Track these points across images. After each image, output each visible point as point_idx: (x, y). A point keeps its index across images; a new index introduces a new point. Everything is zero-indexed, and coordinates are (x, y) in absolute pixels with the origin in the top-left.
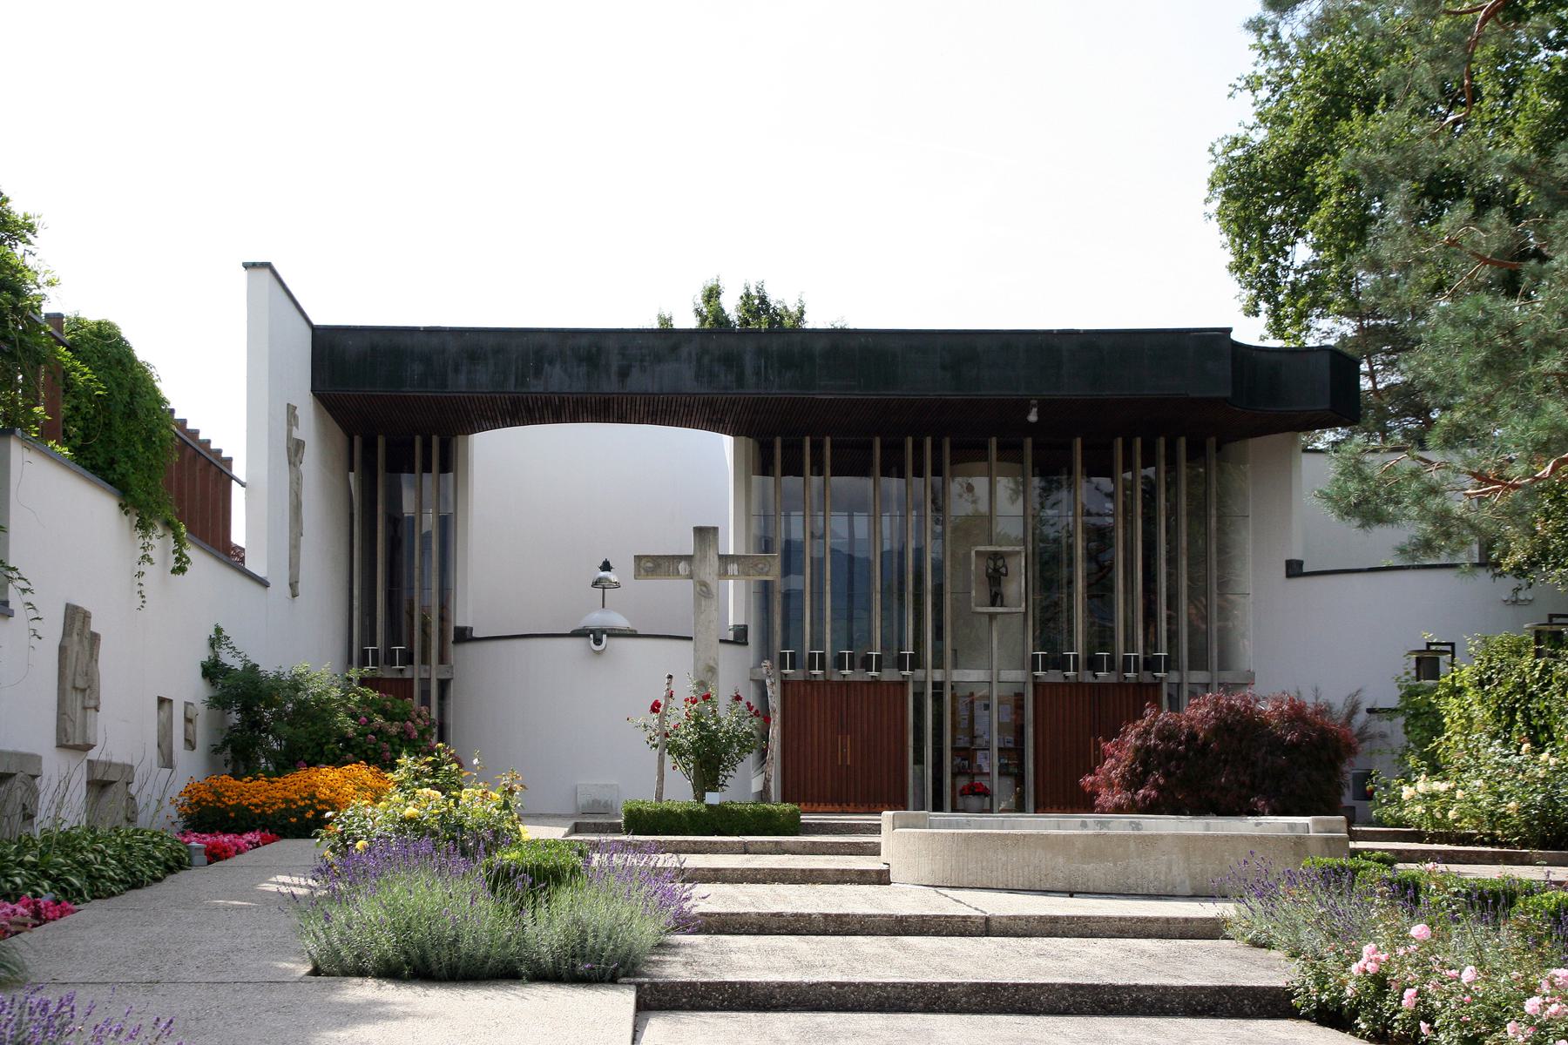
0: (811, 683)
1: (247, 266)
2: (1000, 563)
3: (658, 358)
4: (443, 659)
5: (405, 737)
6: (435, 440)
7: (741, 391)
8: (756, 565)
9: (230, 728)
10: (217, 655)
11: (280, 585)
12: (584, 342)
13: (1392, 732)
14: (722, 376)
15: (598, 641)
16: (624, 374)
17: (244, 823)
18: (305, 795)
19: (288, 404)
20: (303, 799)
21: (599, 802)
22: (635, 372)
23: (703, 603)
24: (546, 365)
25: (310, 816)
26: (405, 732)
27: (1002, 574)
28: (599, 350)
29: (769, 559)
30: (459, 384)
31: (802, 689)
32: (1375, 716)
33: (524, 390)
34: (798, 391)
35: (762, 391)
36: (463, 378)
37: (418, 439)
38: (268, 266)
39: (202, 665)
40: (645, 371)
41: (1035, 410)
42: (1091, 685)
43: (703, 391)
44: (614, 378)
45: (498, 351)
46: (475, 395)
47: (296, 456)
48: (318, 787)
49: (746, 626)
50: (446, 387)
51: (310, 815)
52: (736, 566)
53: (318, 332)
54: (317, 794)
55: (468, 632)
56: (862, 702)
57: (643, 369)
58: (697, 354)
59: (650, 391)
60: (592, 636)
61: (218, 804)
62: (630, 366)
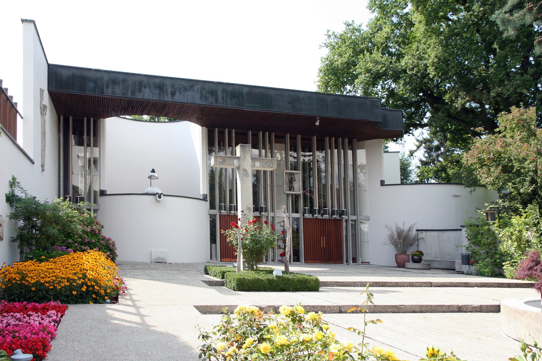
0: (229, 216)
1: (23, 21)
2: (293, 176)
3: (186, 90)
4: (95, 202)
5: (93, 233)
6: (92, 119)
7: (216, 105)
8: (267, 163)
9: (19, 228)
10: (13, 191)
11: (38, 162)
12: (158, 81)
13: (426, 237)
14: (210, 98)
15: (160, 197)
16: (173, 94)
17: (40, 293)
18: (81, 276)
19: (40, 89)
20: (79, 279)
21: (160, 258)
22: (177, 94)
23: (245, 178)
24: (143, 88)
25: (85, 290)
26: (93, 231)
27: (294, 180)
28: (164, 85)
29: (273, 161)
30: (109, 92)
31: (226, 218)
32: (419, 232)
33: (135, 97)
34: (237, 107)
35: (225, 105)
36: (110, 90)
37: (85, 119)
38: (33, 22)
39: (6, 196)
40: (181, 94)
41: (319, 121)
42: (320, 219)
43: (203, 103)
44: (169, 96)
45: (124, 81)
46: (115, 97)
47: (44, 111)
48: (87, 270)
49: (207, 195)
50: (103, 93)
51: (84, 289)
52: (259, 163)
53: (50, 67)
54: (87, 274)
55: (105, 192)
56: (316, 223)
57: (180, 93)
58: (200, 89)
59: (183, 102)
60: (157, 195)
61: (23, 282)
62: (175, 92)
